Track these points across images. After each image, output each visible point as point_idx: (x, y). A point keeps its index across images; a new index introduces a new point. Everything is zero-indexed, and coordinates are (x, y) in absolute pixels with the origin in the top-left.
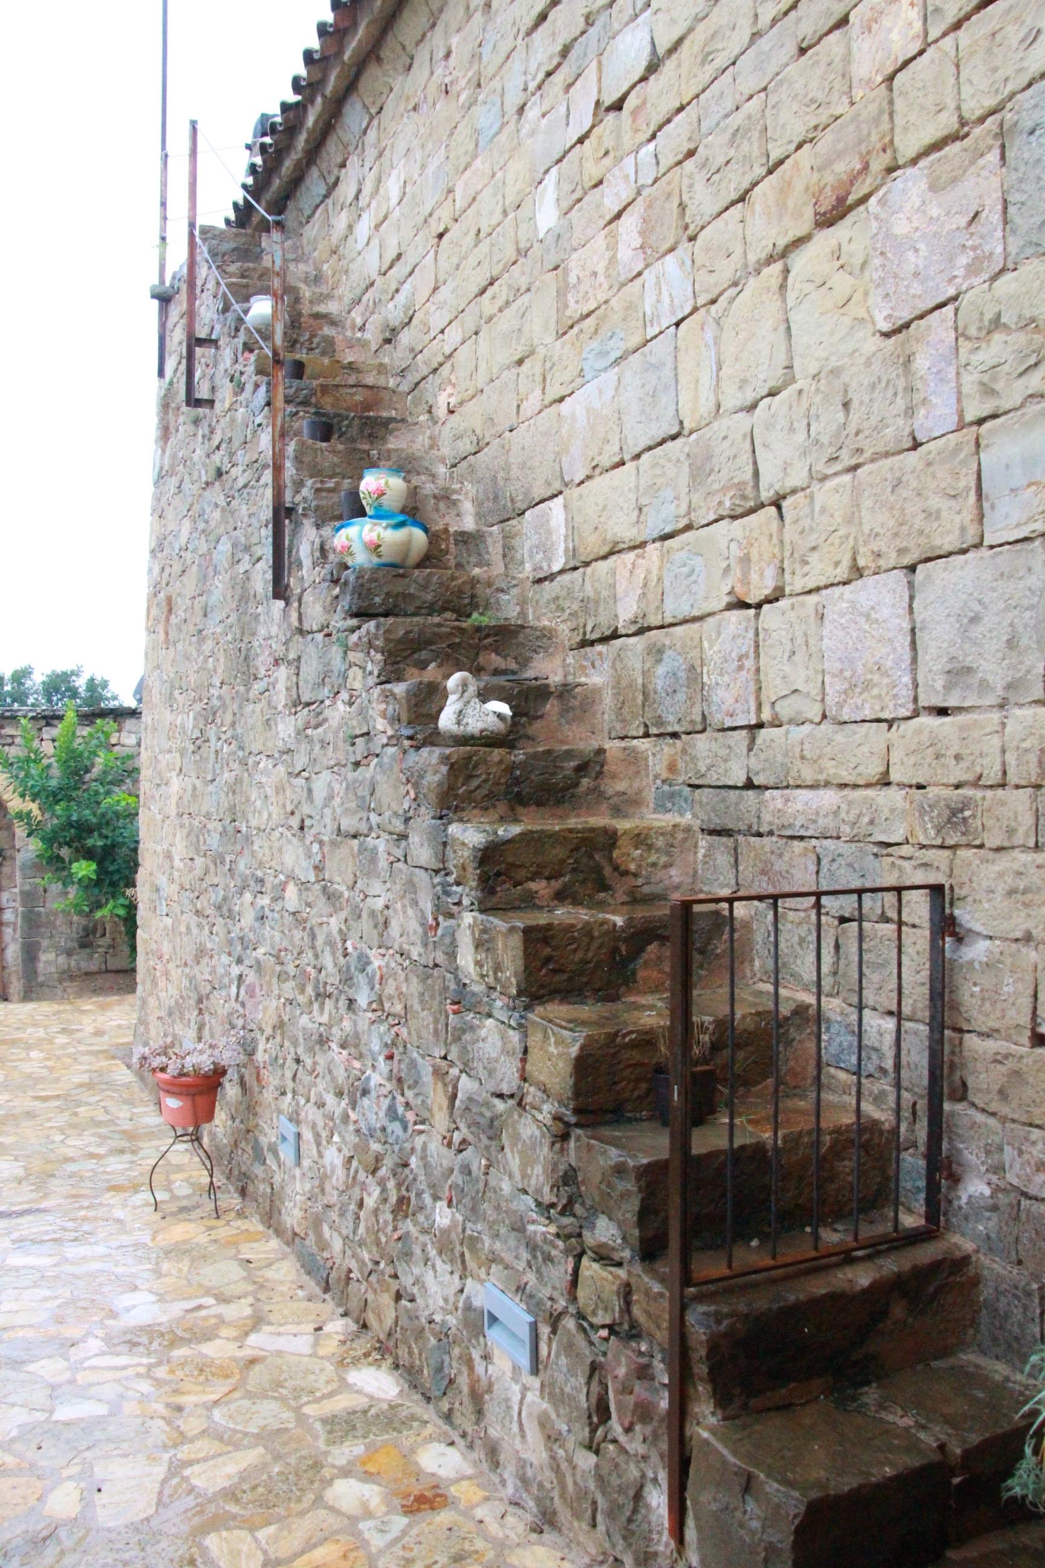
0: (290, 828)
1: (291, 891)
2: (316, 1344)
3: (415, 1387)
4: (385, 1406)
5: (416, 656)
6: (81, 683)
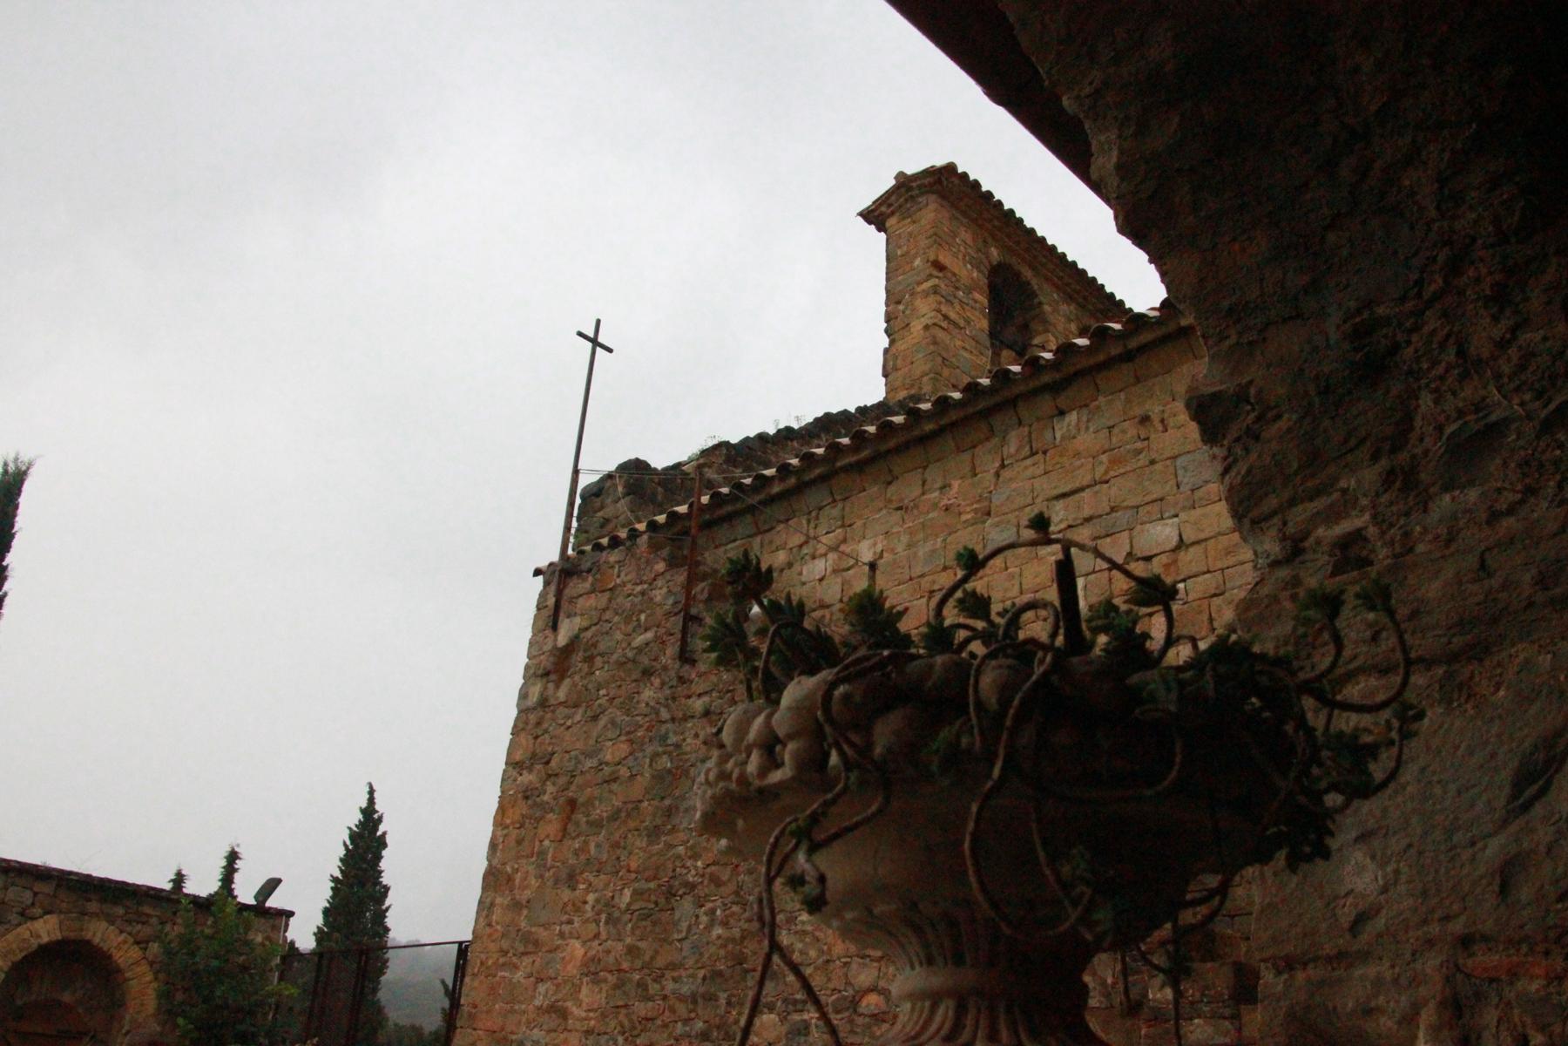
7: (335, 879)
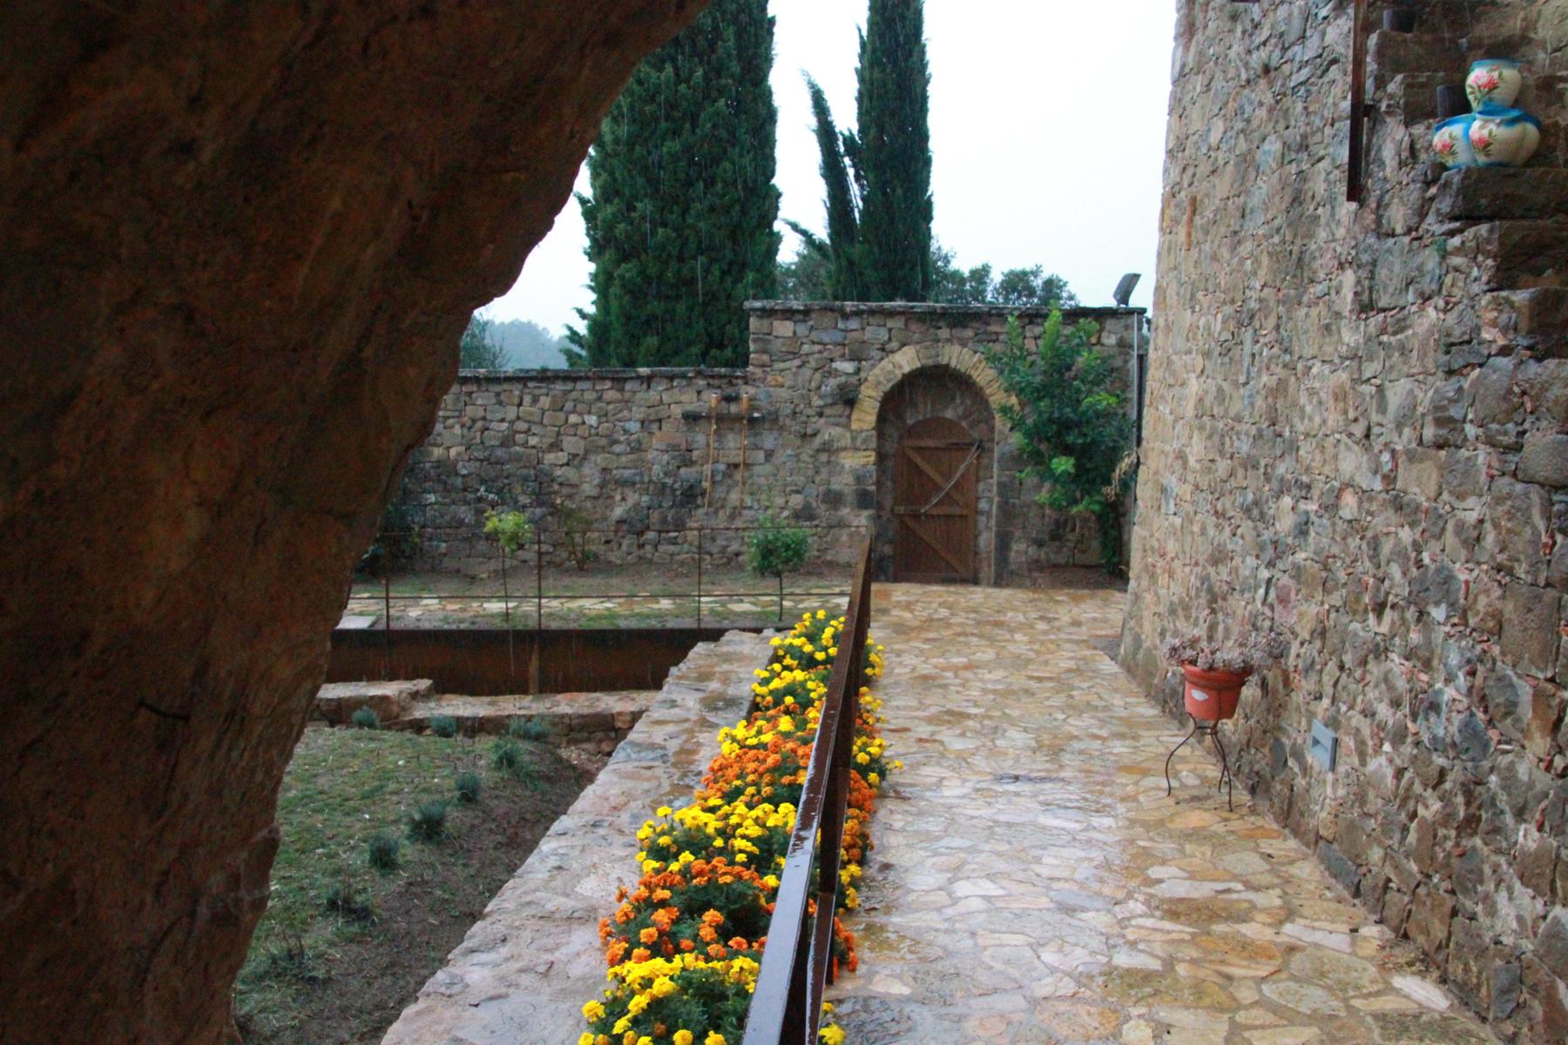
0: (1350, 435)
2: (1353, 943)
3: (1467, 1004)
4: (1437, 1016)
5: (1532, 262)
6: (1038, 283)
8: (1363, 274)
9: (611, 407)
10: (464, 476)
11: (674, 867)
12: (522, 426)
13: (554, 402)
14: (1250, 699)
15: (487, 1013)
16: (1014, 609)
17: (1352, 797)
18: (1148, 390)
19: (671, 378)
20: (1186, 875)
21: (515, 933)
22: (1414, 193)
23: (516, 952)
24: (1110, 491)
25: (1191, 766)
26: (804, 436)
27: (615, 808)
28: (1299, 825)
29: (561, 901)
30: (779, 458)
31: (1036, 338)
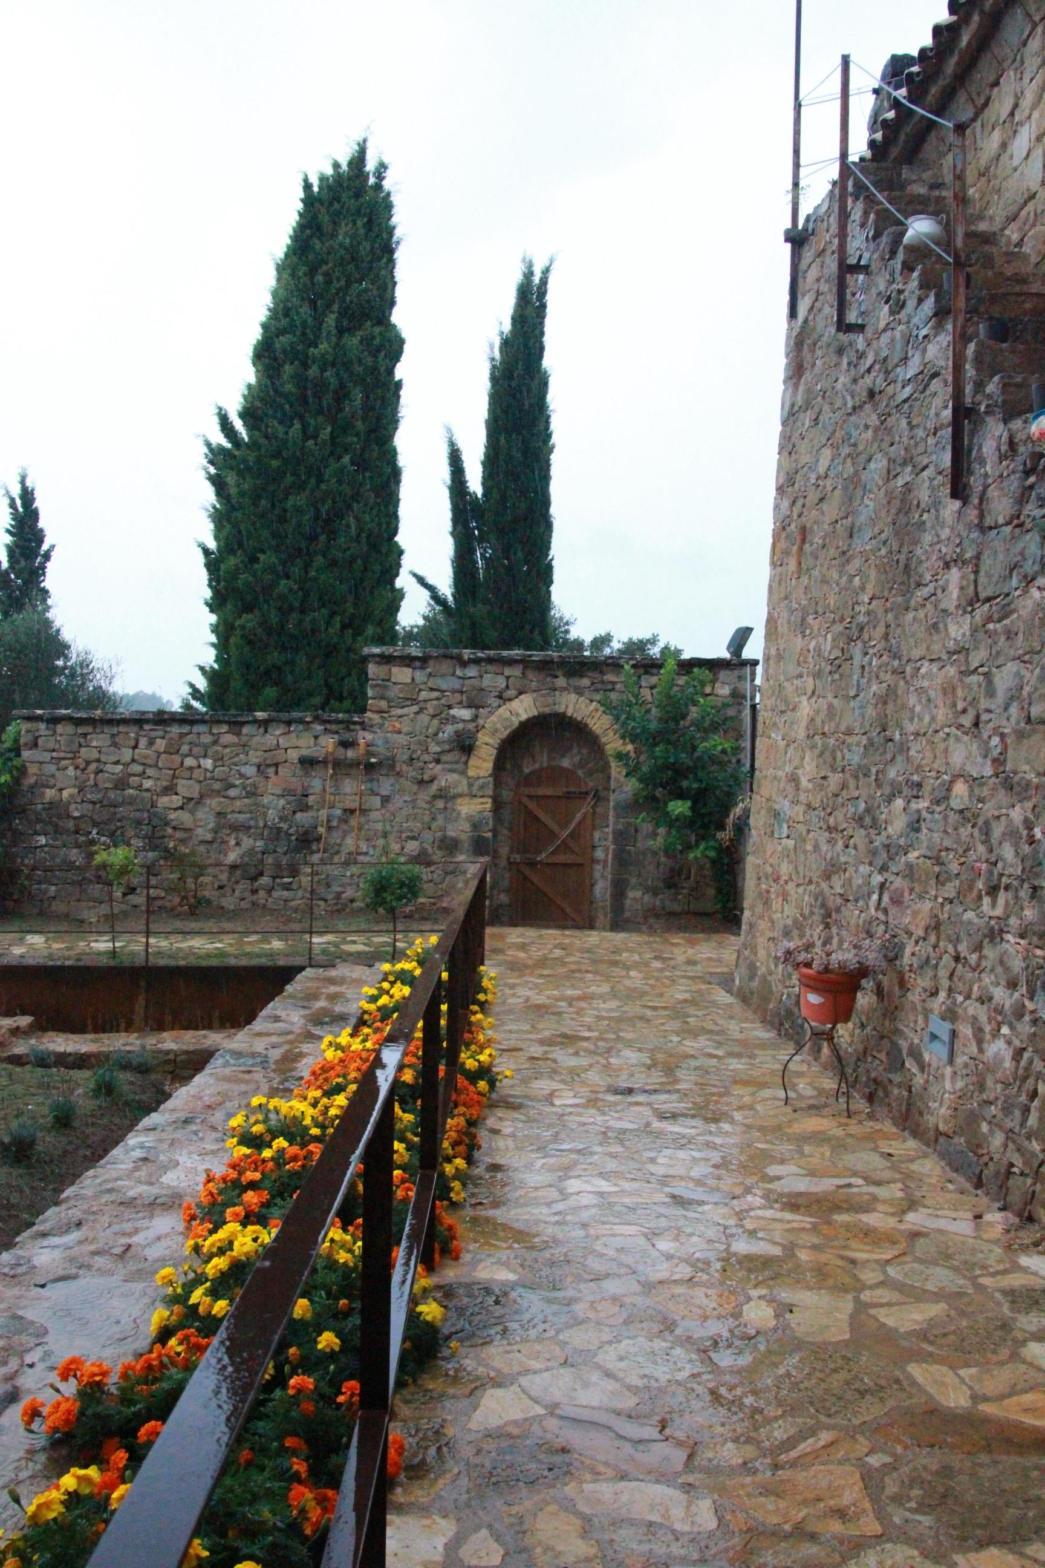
0: (960, 726)
1: (960, 788)
2: (977, 1228)
7: (249, 387)
8: (970, 569)
9: (228, 750)
10: (76, 818)
11: (267, 1153)
12: (137, 768)
13: (167, 746)
14: (866, 1007)
15: (56, 1292)
16: (631, 951)
17: (971, 1087)
18: (760, 719)
19: (289, 723)
20: (804, 1172)
21: (91, 1218)
22: (1014, 484)
23: (91, 1235)
24: (724, 836)
25: (808, 1080)
26: (421, 782)
27: (209, 1107)
28: (918, 1125)
29: (143, 1189)
30: (398, 802)
31: (652, 688)
